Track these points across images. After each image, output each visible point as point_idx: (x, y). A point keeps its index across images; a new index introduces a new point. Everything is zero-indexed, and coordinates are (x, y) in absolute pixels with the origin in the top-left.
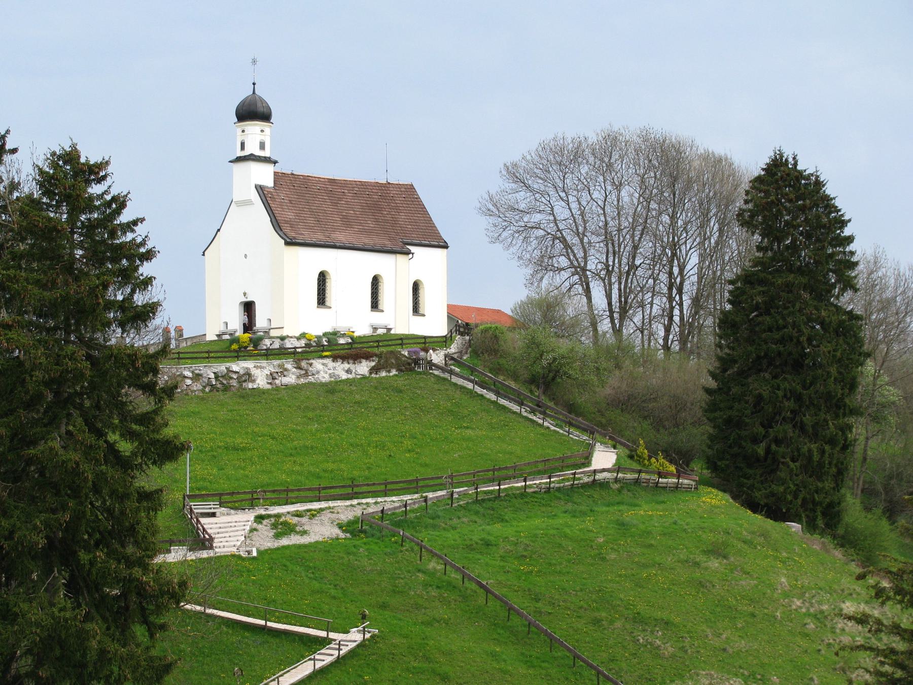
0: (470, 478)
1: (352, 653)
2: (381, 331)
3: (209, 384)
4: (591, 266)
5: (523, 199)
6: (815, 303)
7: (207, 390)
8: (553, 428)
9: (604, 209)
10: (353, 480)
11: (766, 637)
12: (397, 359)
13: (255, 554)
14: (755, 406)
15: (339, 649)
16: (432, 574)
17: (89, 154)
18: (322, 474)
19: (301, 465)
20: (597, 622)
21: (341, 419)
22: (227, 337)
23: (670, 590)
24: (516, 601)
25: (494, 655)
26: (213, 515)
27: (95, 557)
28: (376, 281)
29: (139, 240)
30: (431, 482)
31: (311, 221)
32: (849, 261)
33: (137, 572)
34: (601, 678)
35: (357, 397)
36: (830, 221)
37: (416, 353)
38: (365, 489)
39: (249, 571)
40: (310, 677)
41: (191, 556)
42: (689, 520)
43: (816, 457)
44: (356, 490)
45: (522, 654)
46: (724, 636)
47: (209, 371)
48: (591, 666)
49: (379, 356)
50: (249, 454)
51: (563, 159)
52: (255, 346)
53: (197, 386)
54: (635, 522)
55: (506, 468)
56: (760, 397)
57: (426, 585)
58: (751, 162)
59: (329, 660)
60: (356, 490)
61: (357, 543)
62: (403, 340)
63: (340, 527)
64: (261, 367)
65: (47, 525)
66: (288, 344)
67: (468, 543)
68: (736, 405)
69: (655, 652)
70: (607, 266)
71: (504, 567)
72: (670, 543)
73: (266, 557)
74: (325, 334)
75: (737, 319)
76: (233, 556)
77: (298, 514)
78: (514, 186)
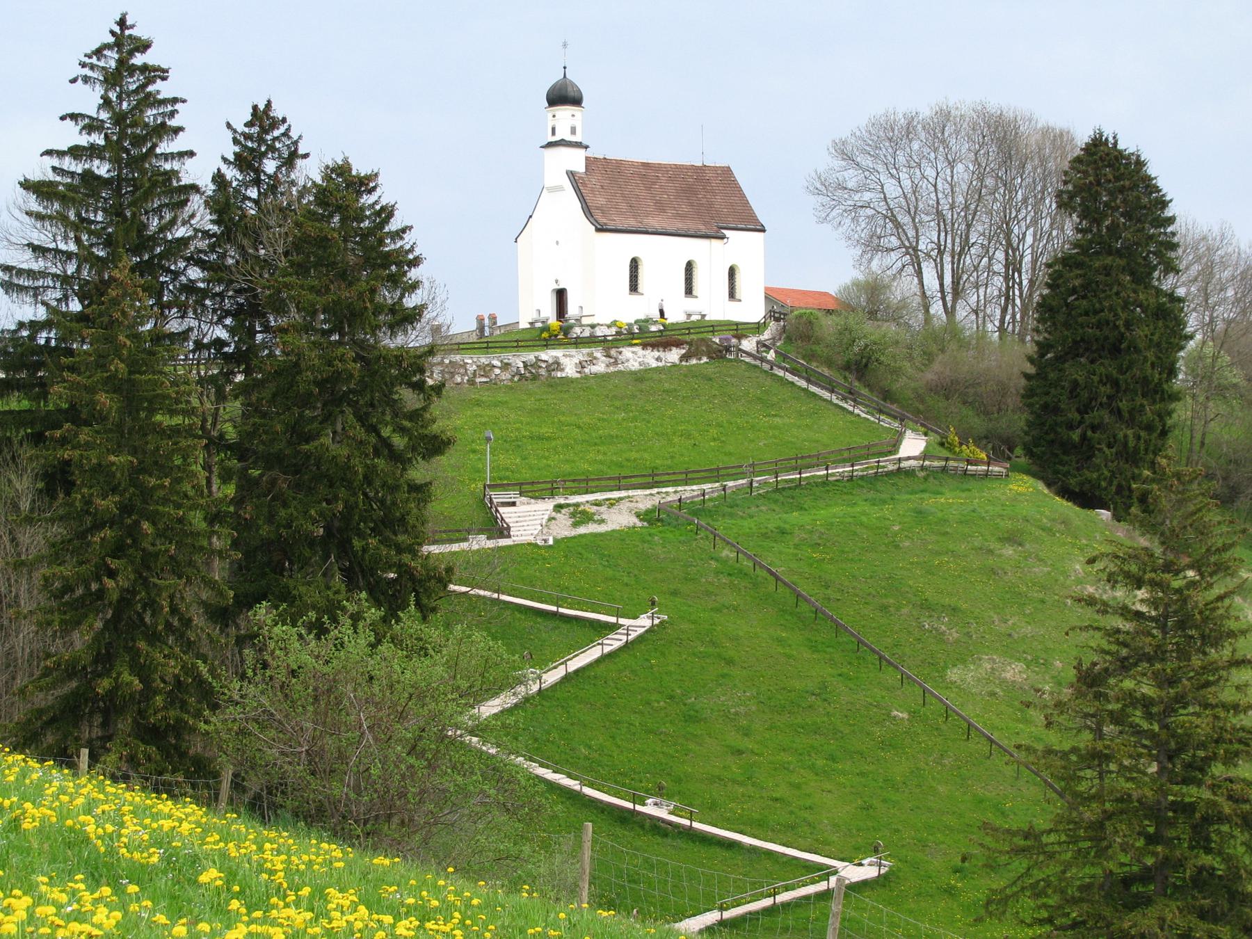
0: (773, 467)
1: (641, 639)
2: (694, 318)
3: (518, 373)
4: (922, 246)
5: (852, 178)
6: (1134, 286)
7: (516, 379)
8: (863, 415)
9: (935, 186)
10: (654, 468)
11: (1053, 624)
12: (708, 346)
13: (551, 542)
14: (1071, 392)
15: (628, 635)
16: (725, 561)
17: (360, 167)
18: (625, 463)
19: (605, 454)
20: (884, 608)
21: (649, 407)
22: (539, 325)
23: (960, 576)
24: (804, 588)
25: (780, 641)
26: (513, 504)
27: (367, 544)
28: (689, 267)
29: (407, 247)
30: (734, 471)
31: (623, 206)
32: (1170, 242)
33: (406, 558)
34: (884, 663)
35: (667, 385)
36: (1150, 202)
37: (728, 340)
38: (666, 478)
39: (544, 559)
40: (598, 662)
41: (491, 544)
42: (990, 508)
43: (1132, 443)
44: (656, 479)
45: (809, 640)
46: (1010, 623)
47: (518, 360)
48: (873, 651)
49: (690, 343)
50: (554, 443)
51: (894, 136)
52: (566, 334)
53: (506, 376)
54: (933, 510)
55: (809, 456)
56: (1075, 384)
57: (717, 573)
58: (1083, 136)
59: (617, 644)
60: (656, 479)
61: (652, 531)
62: (715, 327)
63: (638, 515)
64: (570, 356)
65: (321, 514)
66: (599, 332)
67: (764, 531)
68: (1053, 391)
69: (940, 637)
70: (939, 246)
71: (796, 555)
72: (966, 530)
73: (563, 546)
74: (636, 322)
75: (1054, 304)
76: (529, 544)
77: (597, 504)
78: (844, 163)
